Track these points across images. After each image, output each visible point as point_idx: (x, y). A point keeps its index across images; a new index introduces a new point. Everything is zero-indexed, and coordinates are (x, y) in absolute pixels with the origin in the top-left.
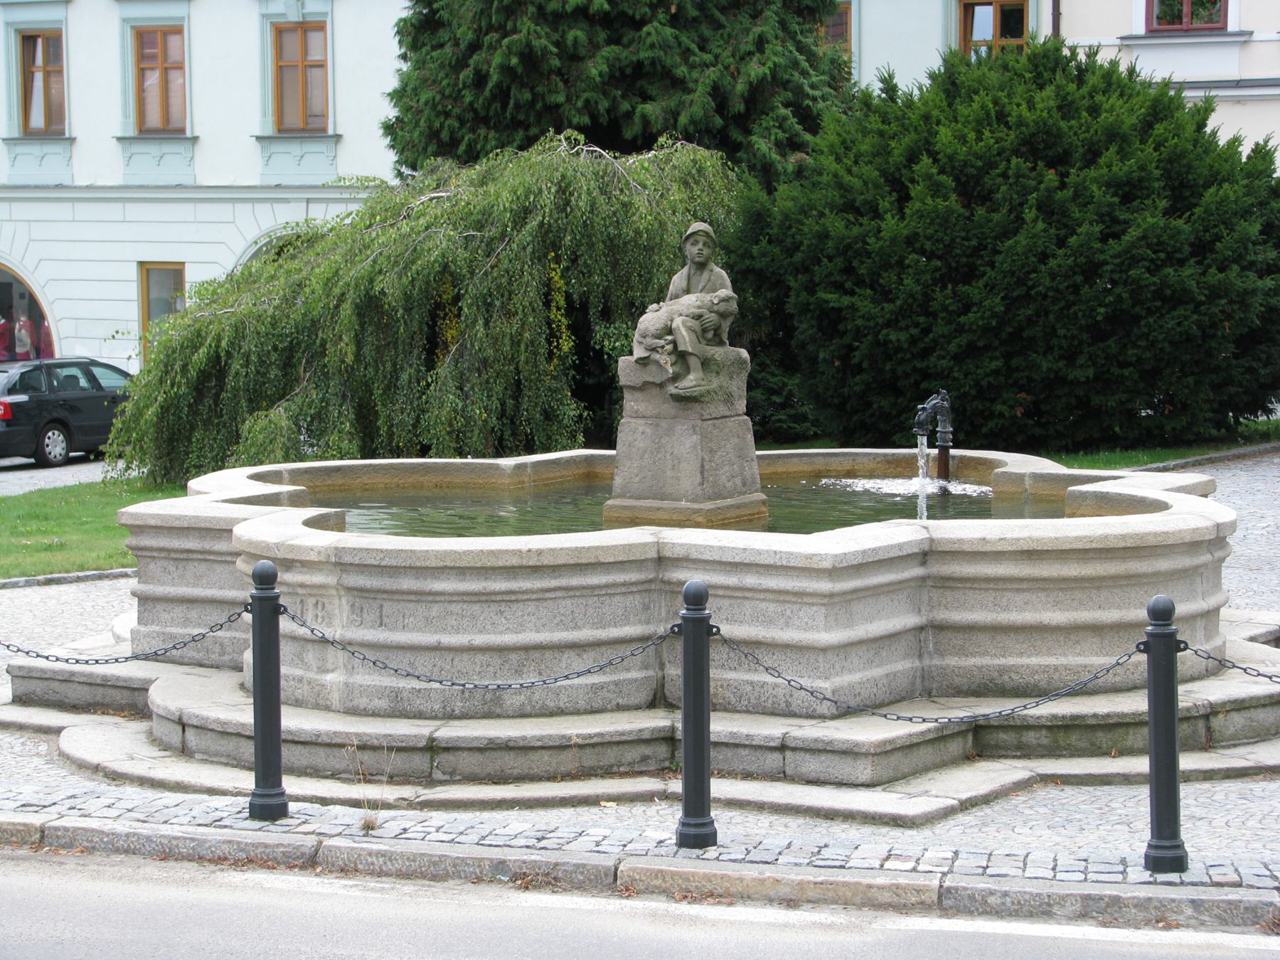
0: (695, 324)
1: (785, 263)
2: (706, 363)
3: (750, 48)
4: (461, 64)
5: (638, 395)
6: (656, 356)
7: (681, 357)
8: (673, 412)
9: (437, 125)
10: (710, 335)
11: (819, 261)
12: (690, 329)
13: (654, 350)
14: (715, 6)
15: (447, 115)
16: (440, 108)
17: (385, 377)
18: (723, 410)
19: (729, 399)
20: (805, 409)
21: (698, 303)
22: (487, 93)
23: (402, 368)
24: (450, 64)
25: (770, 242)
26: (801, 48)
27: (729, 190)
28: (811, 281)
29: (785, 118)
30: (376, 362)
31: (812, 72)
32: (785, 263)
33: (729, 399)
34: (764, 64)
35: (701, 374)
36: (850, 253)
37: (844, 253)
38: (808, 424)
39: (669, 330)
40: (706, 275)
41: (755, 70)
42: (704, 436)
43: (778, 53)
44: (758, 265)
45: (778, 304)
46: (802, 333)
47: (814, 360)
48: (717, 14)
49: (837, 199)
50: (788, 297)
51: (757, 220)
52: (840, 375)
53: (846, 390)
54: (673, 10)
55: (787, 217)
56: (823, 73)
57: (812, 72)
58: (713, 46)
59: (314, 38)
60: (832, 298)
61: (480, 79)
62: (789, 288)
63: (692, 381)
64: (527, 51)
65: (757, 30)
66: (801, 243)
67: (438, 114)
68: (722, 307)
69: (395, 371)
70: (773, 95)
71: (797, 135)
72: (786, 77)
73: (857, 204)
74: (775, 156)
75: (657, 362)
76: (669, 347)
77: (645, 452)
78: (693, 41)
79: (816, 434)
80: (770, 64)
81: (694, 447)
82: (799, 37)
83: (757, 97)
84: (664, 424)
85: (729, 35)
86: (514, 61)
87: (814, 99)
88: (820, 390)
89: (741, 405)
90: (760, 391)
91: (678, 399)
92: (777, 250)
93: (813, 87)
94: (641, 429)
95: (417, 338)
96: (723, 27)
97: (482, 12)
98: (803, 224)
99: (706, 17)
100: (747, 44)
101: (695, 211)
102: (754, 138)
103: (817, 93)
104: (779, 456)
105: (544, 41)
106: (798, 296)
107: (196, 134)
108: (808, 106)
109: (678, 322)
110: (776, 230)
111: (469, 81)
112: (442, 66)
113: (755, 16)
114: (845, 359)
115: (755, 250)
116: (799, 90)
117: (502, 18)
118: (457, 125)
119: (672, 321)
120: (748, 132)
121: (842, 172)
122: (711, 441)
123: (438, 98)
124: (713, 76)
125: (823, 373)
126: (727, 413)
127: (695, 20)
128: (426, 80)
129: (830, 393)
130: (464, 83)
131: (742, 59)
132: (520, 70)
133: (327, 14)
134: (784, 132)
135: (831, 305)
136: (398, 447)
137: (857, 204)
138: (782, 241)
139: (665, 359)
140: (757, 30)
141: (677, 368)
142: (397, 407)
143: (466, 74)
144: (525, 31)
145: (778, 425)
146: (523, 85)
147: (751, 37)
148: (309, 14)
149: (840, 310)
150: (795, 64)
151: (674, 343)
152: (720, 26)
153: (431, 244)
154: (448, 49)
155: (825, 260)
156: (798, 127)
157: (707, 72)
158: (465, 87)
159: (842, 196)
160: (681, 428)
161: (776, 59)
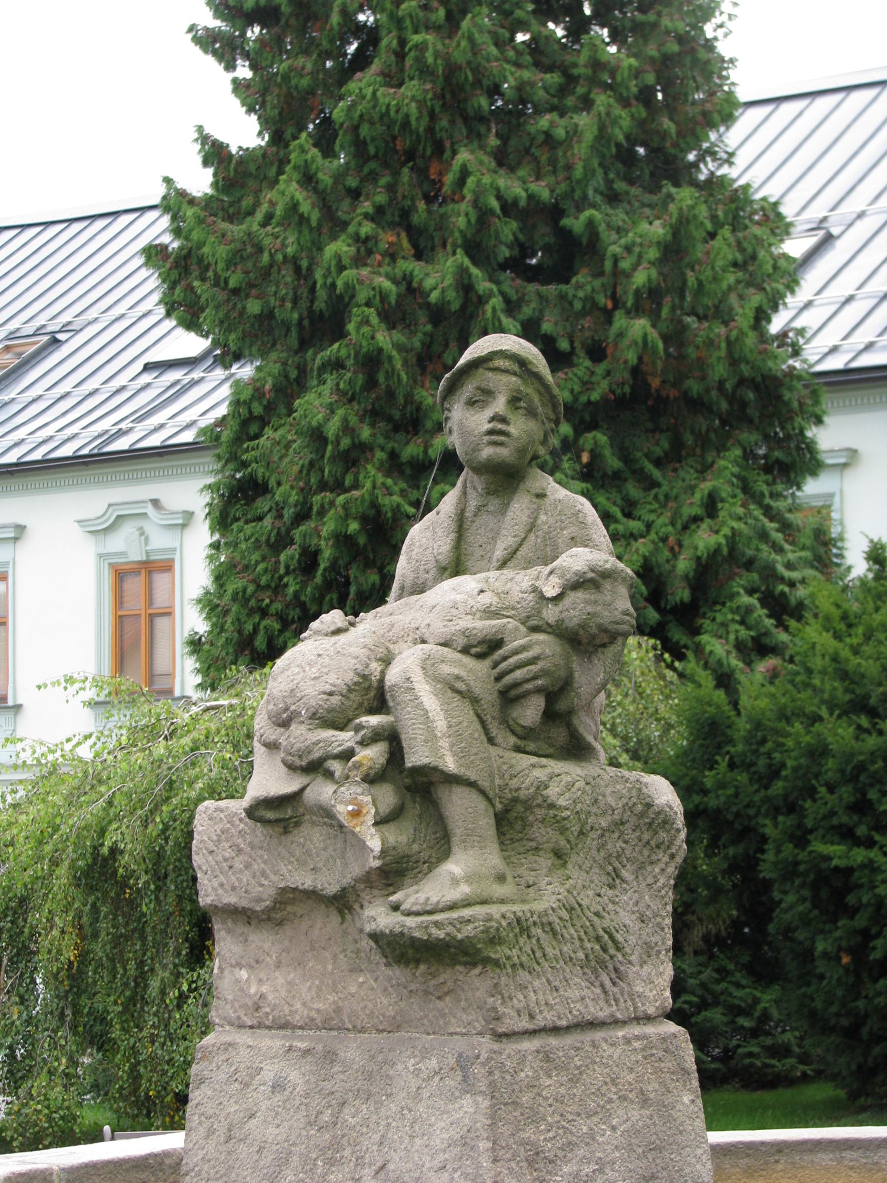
0: (476, 673)
1: (757, 798)
2: (513, 819)
3: (697, 511)
4: (281, 541)
5: (263, 941)
6: (322, 792)
7: (417, 789)
8: (385, 1004)
9: (249, 627)
10: (530, 712)
11: (812, 792)
12: (452, 688)
13: (315, 768)
14: (647, 456)
15: (264, 613)
16: (253, 603)
17: (126, 985)
18: (580, 997)
19: (604, 957)
20: (789, 1037)
21: (487, 599)
22: (318, 579)
23: (152, 970)
24: (268, 541)
25: (732, 766)
26: (768, 511)
27: (668, 697)
28: (800, 826)
29: (749, 610)
30: (112, 960)
31: (787, 547)
32: (757, 798)
33: (604, 957)
34: (717, 532)
35: (493, 859)
36: (863, 778)
37: (854, 778)
38: (792, 1061)
39: (378, 698)
40: (519, 508)
41: (705, 539)
42: (503, 1101)
43: (736, 517)
44: (712, 802)
45: (745, 867)
46: (786, 911)
47: (807, 956)
48: (649, 467)
49: (839, 693)
50: (763, 851)
51: (710, 734)
52: (851, 979)
53: (861, 1004)
54: (585, 458)
55: (758, 725)
56: (803, 548)
57: (787, 547)
58: (642, 511)
59: (160, 580)
60: (836, 852)
61: (309, 560)
62: (764, 839)
63: (457, 883)
64: (372, 512)
65: (706, 486)
66: (783, 765)
67: (251, 612)
68: (575, 610)
69: (143, 973)
70: (731, 578)
71: (767, 634)
72: (750, 553)
73: (873, 701)
74: (735, 662)
75: (327, 813)
76: (372, 755)
77: (283, 1161)
78: (614, 503)
79: (804, 1074)
80: (726, 531)
81: (466, 1143)
82: (767, 500)
83: (708, 577)
84: (352, 1051)
85: (667, 496)
86: (354, 526)
87: (792, 584)
88: (818, 1004)
89: (654, 981)
90: (719, 1010)
91: (407, 952)
92: (742, 778)
93: (789, 566)
94: (269, 1073)
95: (175, 920)
96: (659, 485)
97: (312, 464)
98: (788, 735)
99: (634, 472)
100: (692, 506)
101: (613, 725)
102: (704, 638)
103: (795, 575)
104: (781, 1147)
105: (396, 499)
106: (778, 851)
107: (19, 702)
108: (783, 594)
109: (407, 667)
110: (740, 747)
111: (294, 564)
112: (257, 545)
113: (704, 469)
114: (859, 951)
115: (709, 779)
116: (770, 574)
117: (339, 469)
118: (277, 626)
119: (387, 661)
120: (696, 631)
121: (845, 653)
122: (534, 1117)
123: (251, 588)
124: (643, 550)
125: (822, 977)
126: (603, 1014)
127: (617, 476)
128: (235, 566)
129: (834, 1009)
130: (287, 567)
131: (685, 527)
132: (362, 540)
133: (174, 550)
134: (748, 628)
135: (835, 862)
136: (148, 1097)
137: (873, 701)
138: (752, 764)
139: (348, 799)
140: (706, 486)
141: (399, 836)
142: (145, 1033)
143: (290, 554)
144: (368, 485)
145: (747, 1061)
146: (368, 564)
147: (698, 496)
148: (153, 551)
149: (848, 871)
150: (763, 536)
151: (393, 739)
152: (652, 484)
153: (192, 773)
154: (268, 522)
155: (823, 790)
156: (769, 622)
157: (635, 545)
158: (287, 573)
159: (846, 691)
160: (417, 1066)
161: (735, 524)
